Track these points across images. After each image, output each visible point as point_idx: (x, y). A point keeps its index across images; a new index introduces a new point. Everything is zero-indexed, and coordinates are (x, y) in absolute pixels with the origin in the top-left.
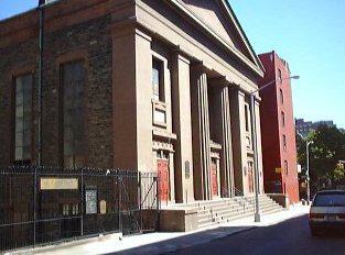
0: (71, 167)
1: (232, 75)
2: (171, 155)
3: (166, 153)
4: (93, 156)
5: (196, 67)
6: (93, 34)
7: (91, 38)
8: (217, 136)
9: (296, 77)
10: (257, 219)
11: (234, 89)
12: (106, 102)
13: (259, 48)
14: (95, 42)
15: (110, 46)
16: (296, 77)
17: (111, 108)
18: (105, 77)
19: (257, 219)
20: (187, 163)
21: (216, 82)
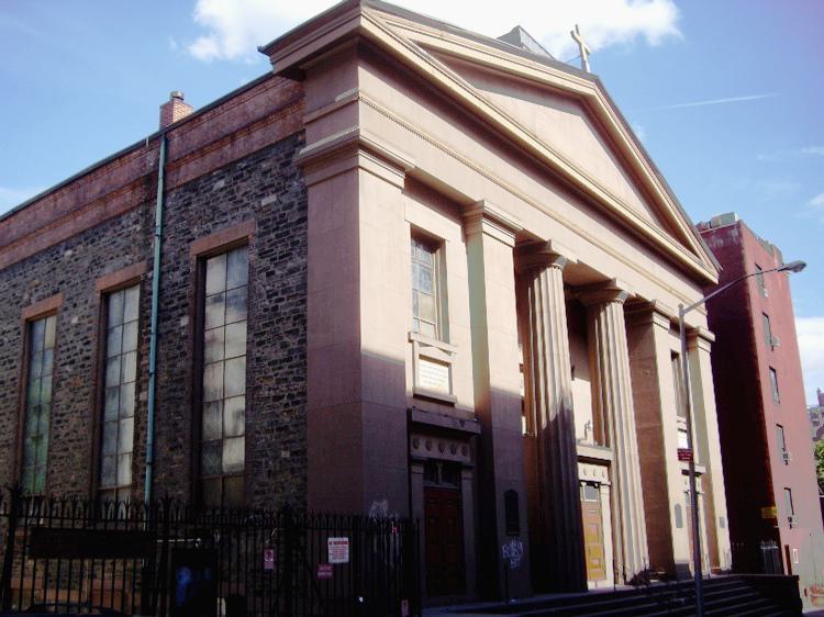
0: (23, 533)
1: (634, 274)
2: (605, 490)
3: (453, 469)
4: (263, 478)
5: (531, 256)
6: (267, 181)
7: (264, 190)
8: (548, 453)
9: (799, 267)
10: (217, 299)
11: (639, 314)
12: (292, 341)
13: (698, 206)
14: (272, 198)
15: (304, 207)
16: (799, 267)
17: (304, 356)
18: (293, 281)
19: (217, 299)
20: (680, 525)
21: (587, 295)
